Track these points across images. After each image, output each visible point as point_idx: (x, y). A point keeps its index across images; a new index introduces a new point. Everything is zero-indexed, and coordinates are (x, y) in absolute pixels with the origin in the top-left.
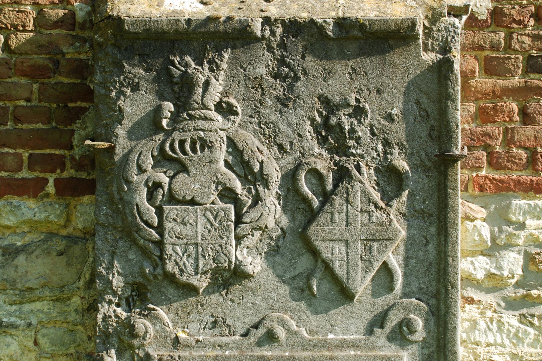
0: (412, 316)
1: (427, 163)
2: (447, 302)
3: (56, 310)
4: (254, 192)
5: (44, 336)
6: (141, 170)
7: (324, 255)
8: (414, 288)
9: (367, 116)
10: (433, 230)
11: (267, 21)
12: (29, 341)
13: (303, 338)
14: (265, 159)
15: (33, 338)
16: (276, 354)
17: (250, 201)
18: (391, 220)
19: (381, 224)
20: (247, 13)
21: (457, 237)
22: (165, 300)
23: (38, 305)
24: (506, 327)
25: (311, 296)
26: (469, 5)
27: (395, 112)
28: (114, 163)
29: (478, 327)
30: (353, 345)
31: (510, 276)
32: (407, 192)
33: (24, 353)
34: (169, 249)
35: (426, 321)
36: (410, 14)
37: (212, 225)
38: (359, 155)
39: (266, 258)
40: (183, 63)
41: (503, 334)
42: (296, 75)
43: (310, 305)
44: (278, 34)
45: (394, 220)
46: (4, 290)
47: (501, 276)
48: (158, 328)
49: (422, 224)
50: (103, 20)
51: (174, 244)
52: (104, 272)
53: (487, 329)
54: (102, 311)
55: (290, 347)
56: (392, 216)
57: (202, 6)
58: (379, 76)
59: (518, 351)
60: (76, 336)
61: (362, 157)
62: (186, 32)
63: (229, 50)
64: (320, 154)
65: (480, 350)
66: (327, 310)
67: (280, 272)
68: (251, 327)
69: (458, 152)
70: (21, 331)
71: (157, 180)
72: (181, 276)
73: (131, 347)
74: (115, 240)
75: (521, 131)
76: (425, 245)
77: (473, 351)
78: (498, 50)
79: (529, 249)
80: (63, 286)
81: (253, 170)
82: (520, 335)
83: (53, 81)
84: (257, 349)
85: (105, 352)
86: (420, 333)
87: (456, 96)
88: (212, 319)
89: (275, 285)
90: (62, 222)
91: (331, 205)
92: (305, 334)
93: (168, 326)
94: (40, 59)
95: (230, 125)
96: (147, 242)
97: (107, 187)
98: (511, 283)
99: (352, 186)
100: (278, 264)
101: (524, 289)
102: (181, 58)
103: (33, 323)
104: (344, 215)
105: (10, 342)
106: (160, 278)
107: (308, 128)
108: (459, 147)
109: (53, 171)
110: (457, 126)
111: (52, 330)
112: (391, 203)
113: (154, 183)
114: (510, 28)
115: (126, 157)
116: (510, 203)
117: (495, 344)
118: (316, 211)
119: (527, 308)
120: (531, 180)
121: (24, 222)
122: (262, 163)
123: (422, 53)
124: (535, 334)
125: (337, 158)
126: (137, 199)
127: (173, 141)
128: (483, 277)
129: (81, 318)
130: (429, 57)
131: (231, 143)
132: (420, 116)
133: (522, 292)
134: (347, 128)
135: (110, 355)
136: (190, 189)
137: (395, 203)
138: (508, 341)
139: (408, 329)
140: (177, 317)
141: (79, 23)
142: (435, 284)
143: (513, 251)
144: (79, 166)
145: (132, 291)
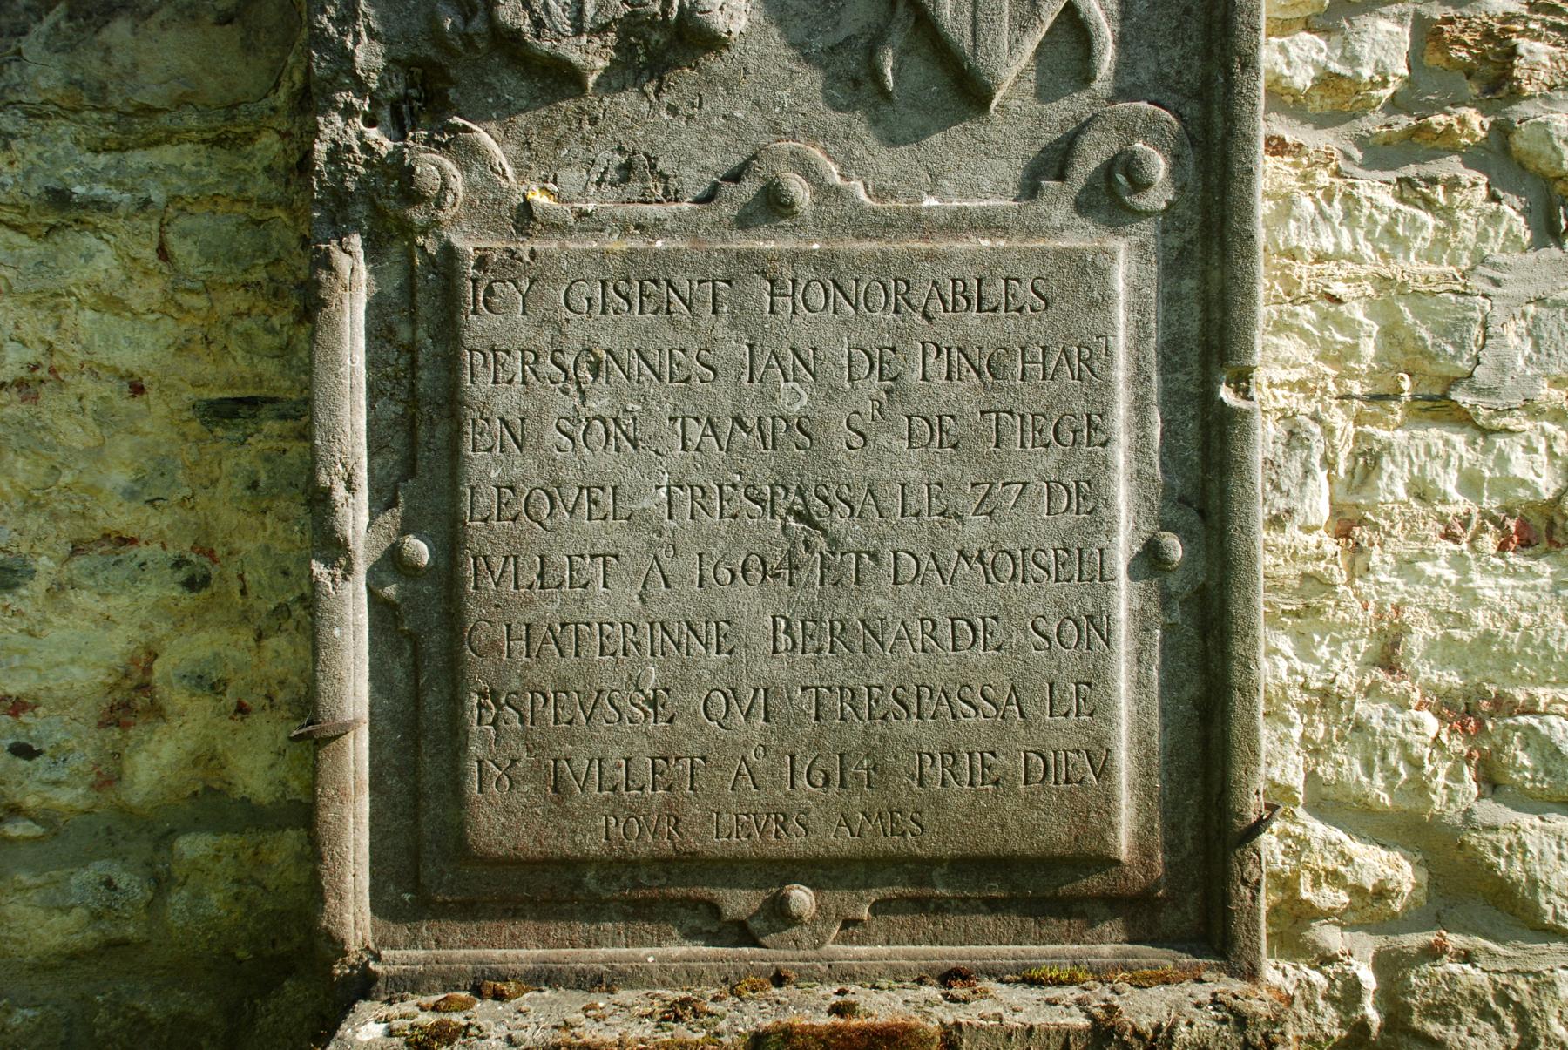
0: (1139, 145)
2: (1229, 106)
3: (216, 166)
5: (184, 235)
8: (1144, 77)
12: (145, 246)
15: (156, 239)
16: (788, 247)
22: (494, 107)
23: (166, 154)
24: (1366, 211)
25: (878, 98)
29: (1296, 211)
30: (988, 224)
31: (1378, 78)
33: (130, 278)
35: (1176, 159)
41: (1358, 230)
43: (875, 122)
46: (76, 111)
47: (1355, 81)
48: (475, 178)
52: (332, 29)
53: (1318, 217)
54: (327, 132)
55: (825, 231)
59: (1392, 270)
60: (269, 236)
65: (1300, 270)
66: (919, 135)
67: (798, 34)
68: (722, 179)
70: (121, 220)
72: (538, 37)
73: (407, 229)
77: (1283, 274)
79: (1425, 10)
80: (235, 105)
82: (1400, 230)
84: (737, 234)
85: (335, 242)
86: (1159, 196)
88: (619, 159)
89: (786, 68)
92: (863, 196)
93: (504, 176)
98: (1380, 99)
100: (792, 12)
101: (1412, 115)
103: (153, 198)
105: (94, 249)
111: (204, 222)
117: (1337, 256)
119: (1416, 162)
124: (1437, 228)
128: (1309, 84)
129: (282, 189)
133: (1404, 121)
135: (349, 248)
138: (1370, 246)
139: (1130, 179)
140: (527, 154)
142: (1197, 64)
143: (1386, 17)
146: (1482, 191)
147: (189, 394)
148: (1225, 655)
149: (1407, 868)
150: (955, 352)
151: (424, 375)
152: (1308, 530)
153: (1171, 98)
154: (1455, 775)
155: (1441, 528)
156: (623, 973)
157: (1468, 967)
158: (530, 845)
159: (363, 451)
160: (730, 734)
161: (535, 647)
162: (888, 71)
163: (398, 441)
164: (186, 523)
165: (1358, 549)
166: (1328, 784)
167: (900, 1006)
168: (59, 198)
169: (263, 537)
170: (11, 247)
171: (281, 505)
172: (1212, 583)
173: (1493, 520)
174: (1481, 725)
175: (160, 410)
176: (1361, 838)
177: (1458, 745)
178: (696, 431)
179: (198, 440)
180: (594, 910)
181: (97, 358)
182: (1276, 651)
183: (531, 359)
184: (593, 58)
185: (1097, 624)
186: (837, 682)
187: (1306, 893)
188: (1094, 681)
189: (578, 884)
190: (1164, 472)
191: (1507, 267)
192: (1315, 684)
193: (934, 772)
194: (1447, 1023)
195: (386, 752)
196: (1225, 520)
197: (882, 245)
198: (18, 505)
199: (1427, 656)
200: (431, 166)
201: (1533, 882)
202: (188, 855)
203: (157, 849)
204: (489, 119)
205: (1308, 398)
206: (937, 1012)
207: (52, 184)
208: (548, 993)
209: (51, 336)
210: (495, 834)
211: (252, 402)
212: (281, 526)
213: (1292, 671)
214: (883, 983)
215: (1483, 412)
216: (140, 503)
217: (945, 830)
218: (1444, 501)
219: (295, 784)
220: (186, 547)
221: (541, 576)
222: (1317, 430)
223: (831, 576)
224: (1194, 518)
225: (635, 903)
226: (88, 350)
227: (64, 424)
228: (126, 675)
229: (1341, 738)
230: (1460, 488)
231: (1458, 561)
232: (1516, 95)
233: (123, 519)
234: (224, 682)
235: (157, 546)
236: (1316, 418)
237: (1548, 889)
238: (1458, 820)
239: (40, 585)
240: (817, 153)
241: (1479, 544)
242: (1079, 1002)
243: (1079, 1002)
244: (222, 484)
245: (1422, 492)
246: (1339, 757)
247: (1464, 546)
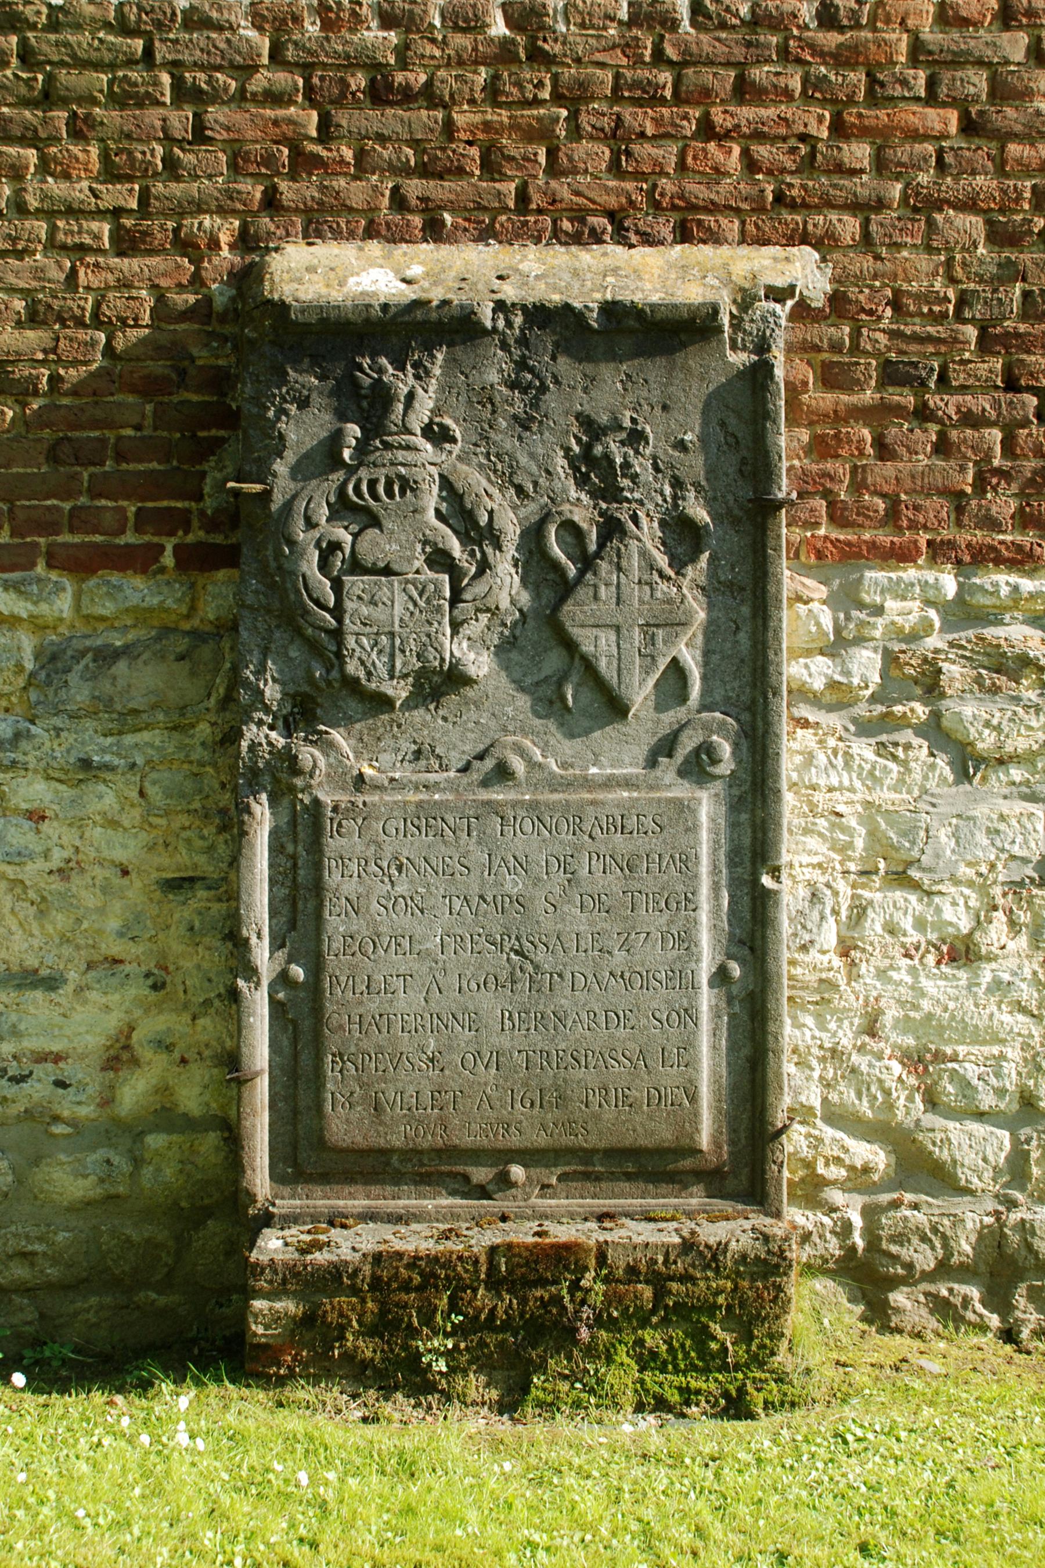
0: (715, 738)
1: (736, 512)
3: (173, 742)
4: (478, 555)
5: (154, 783)
6: (310, 524)
7: (584, 648)
8: (718, 698)
9: (647, 443)
10: (746, 610)
11: (500, 306)
13: (551, 773)
14: (496, 507)
17: (473, 569)
18: (684, 595)
19: (670, 601)
20: (472, 295)
21: (780, 620)
22: (343, 719)
23: (145, 736)
26: (795, 286)
27: (689, 437)
28: (269, 515)
29: (815, 762)
30: (627, 783)
32: (707, 554)
34: (351, 642)
35: (736, 746)
36: (710, 297)
37: (415, 604)
38: (636, 501)
39: (496, 654)
40: (376, 367)
42: (542, 383)
43: (561, 725)
44: (516, 326)
45: (689, 596)
46: (95, 713)
47: (849, 685)
48: (332, 760)
49: (730, 601)
50: (257, 307)
51: (358, 634)
52: (252, 678)
54: (248, 735)
56: (685, 591)
57: (404, 286)
58: (666, 385)
59: (875, 797)
61: (641, 503)
62: (380, 322)
63: (444, 348)
64: (578, 499)
65: (818, 797)
66: (587, 732)
67: (517, 675)
69: (781, 495)
71: (333, 538)
73: (292, 789)
74: (269, 630)
75: (876, 470)
76: (735, 633)
78: (840, 352)
79: (889, 645)
80: (185, 707)
81: (477, 523)
82: (877, 773)
83: (175, 399)
86: (726, 766)
87: (777, 413)
88: (414, 747)
90: (184, 610)
91: (595, 574)
92: (555, 768)
94: (159, 367)
95: (444, 457)
96: (317, 632)
97: (258, 551)
99: (626, 546)
102: (372, 360)
104: (613, 589)
106: (336, 685)
107: (560, 462)
108: (784, 488)
109: (172, 533)
110: (780, 457)
111: (166, 775)
112: (683, 571)
113: (330, 543)
114: (858, 320)
115: (288, 506)
116: (862, 576)
117: (841, 788)
118: (572, 583)
120: (892, 542)
121: (127, 610)
122: (491, 513)
123: (728, 352)
125: (604, 506)
126: (304, 567)
127: (359, 481)
130: (740, 359)
131: (446, 483)
132: (727, 443)
133: (880, 709)
134: (619, 460)
136: (383, 551)
137: (689, 570)
139: (709, 757)
141: (218, 313)
144: (212, 525)
145: (294, 706)
146: (925, 751)
147: (155, 875)
148: (764, 1032)
149: (882, 1154)
150: (608, 858)
151: (301, 872)
152: (824, 952)
153: (733, 711)
154: (910, 1099)
155: (903, 951)
156: (414, 1214)
157: (916, 1212)
158: (360, 1141)
159: (266, 916)
160: (476, 1078)
161: (364, 1028)
162: (569, 697)
163: (286, 910)
164: (151, 951)
165: (853, 964)
166: (835, 1105)
167: (573, 1232)
168: (86, 764)
169: (196, 959)
170: (57, 791)
171: (207, 940)
172: (758, 990)
173: (934, 946)
174: (926, 1069)
175: (138, 884)
176: (855, 1137)
177: (912, 1081)
178: (457, 904)
179: (159, 902)
180: (397, 1178)
181: (103, 855)
182: (804, 1025)
183: (363, 863)
184: (399, 691)
185: (690, 1013)
186: (539, 1048)
187: (821, 1170)
188: (688, 1046)
189: (388, 1164)
190: (730, 925)
191: (940, 796)
192: (827, 1045)
193: (595, 1100)
194: (902, 1245)
195: (278, 1089)
196: (764, 954)
197: (566, 796)
198: (57, 941)
199: (894, 1027)
200: (308, 754)
201: (954, 1162)
202: (153, 1146)
203: (134, 1142)
204: (339, 726)
205: (823, 874)
206: (595, 1235)
207: (81, 756)
208: (371, 1225)
209: (78, 843)
210: (341, 1135)
211: (191, 880)
212: (207, 953)
213: (813, 1037)
214: (564, 1220)
215: (926, 882)
216: (125, 940)
217: (601, 1133)
218: (905, 935)
219: (214, 1105)
220: (152, 965)
221: (368, 987)
222: (828, 892)
223: (535, 986)
224: (747, 952)
225: (421, 1174)
226: (98, 850)
227: (83, 893)
228: (117, 1041)
229: (843, 1077)
230: (914, 927)
231: (912, 971)
232: (943, 695)
233: (116, 948)
234: (173, 1045)
235: (135, 964)
236: (828, 885)
237: (963, 1165)
238: (912, 1126)
239: (70, 988)
240: (528, 743)
241: (925, 960)
242: (676, 1230)
243: (676, 1230)
244: (173, 928)
245: (892, 929)
246: (842, 1089)
247: (916, 961)
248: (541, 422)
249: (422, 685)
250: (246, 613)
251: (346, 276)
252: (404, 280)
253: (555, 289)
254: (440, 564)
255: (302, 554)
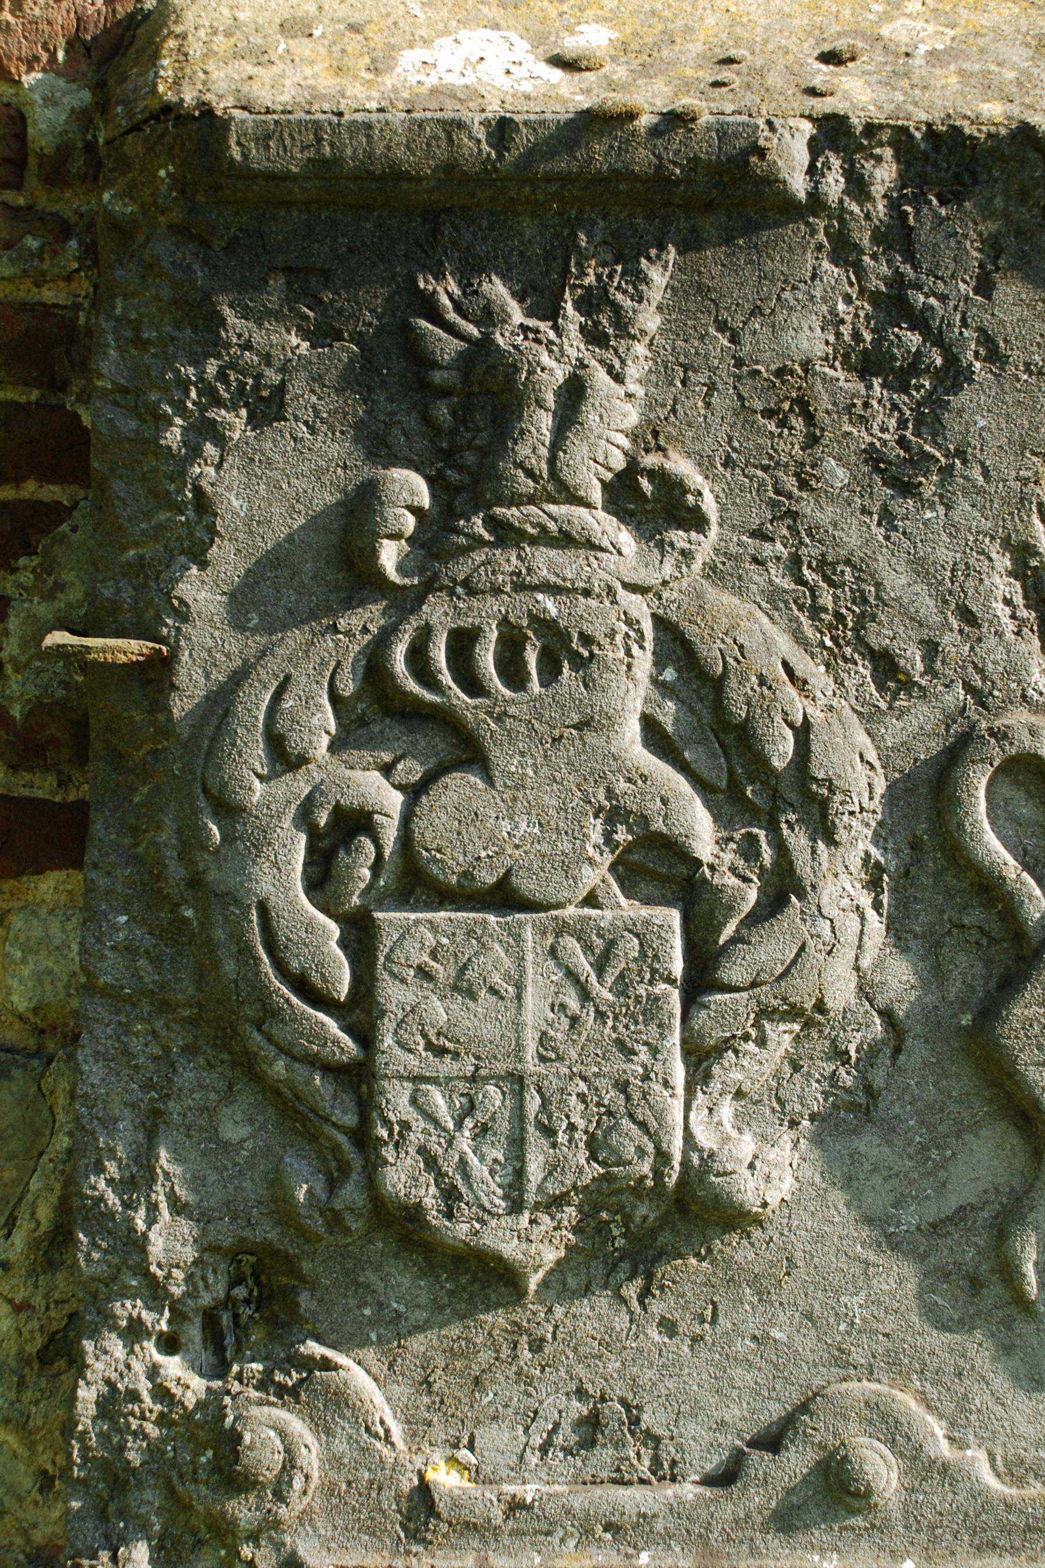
4: (767, 854)
13: (978, 1493)
14: (816, 715)
17: (752, 895)
20: (750, 99)
22: (373, 1323)
28: (167, 729)
37: (585, 995)
39: (818, 1140)
40: (474, 306)
42: (951, 360)
43: (1006, 1350)
44: (878, 190)
48: (340, 1446)
51: (418, 1079)
52: (112, 1199)
54: (98, 1368)
57: (557, 75)
63: (672, 254)
67: (878, 1201)
71: (350, 800)
74: (166, 1060)
88: (578, 1408)
92: (990, 1480)
95: (668, 569)
97: (136, 831)
102: (465, 285)
106: (355, 1225)
113: (339, 813)
122: (803, 732)
126: (265, 884)
136: (492, 839)
141: (41, 156)
145: (233, 1283)
162: (1029, 1270)
248: (947, 472)
249: (603, 1228)
250: (99, 1009)
251: (392, 47)
252: (559, 62)
253: (988, 87)
254: (653, 876)
255: (260, 843)
